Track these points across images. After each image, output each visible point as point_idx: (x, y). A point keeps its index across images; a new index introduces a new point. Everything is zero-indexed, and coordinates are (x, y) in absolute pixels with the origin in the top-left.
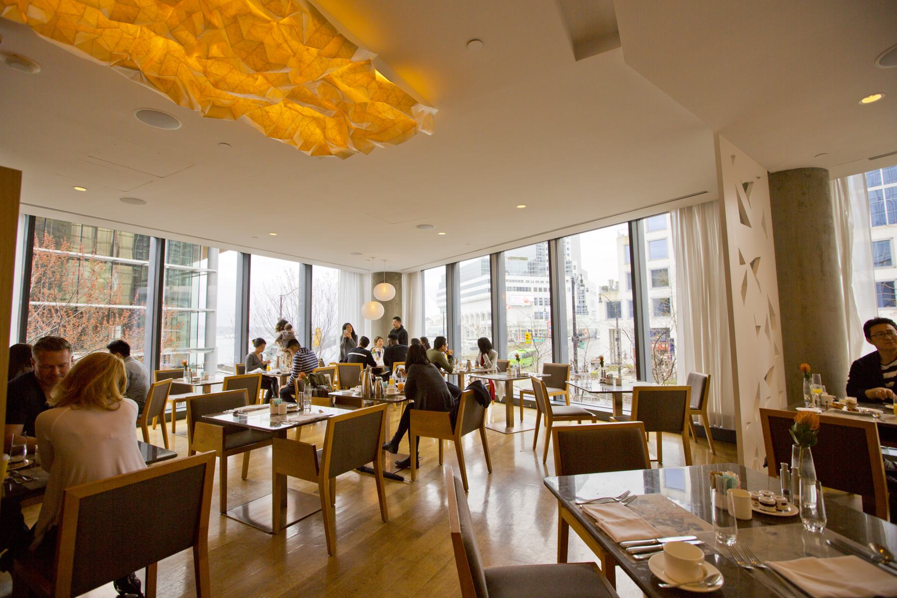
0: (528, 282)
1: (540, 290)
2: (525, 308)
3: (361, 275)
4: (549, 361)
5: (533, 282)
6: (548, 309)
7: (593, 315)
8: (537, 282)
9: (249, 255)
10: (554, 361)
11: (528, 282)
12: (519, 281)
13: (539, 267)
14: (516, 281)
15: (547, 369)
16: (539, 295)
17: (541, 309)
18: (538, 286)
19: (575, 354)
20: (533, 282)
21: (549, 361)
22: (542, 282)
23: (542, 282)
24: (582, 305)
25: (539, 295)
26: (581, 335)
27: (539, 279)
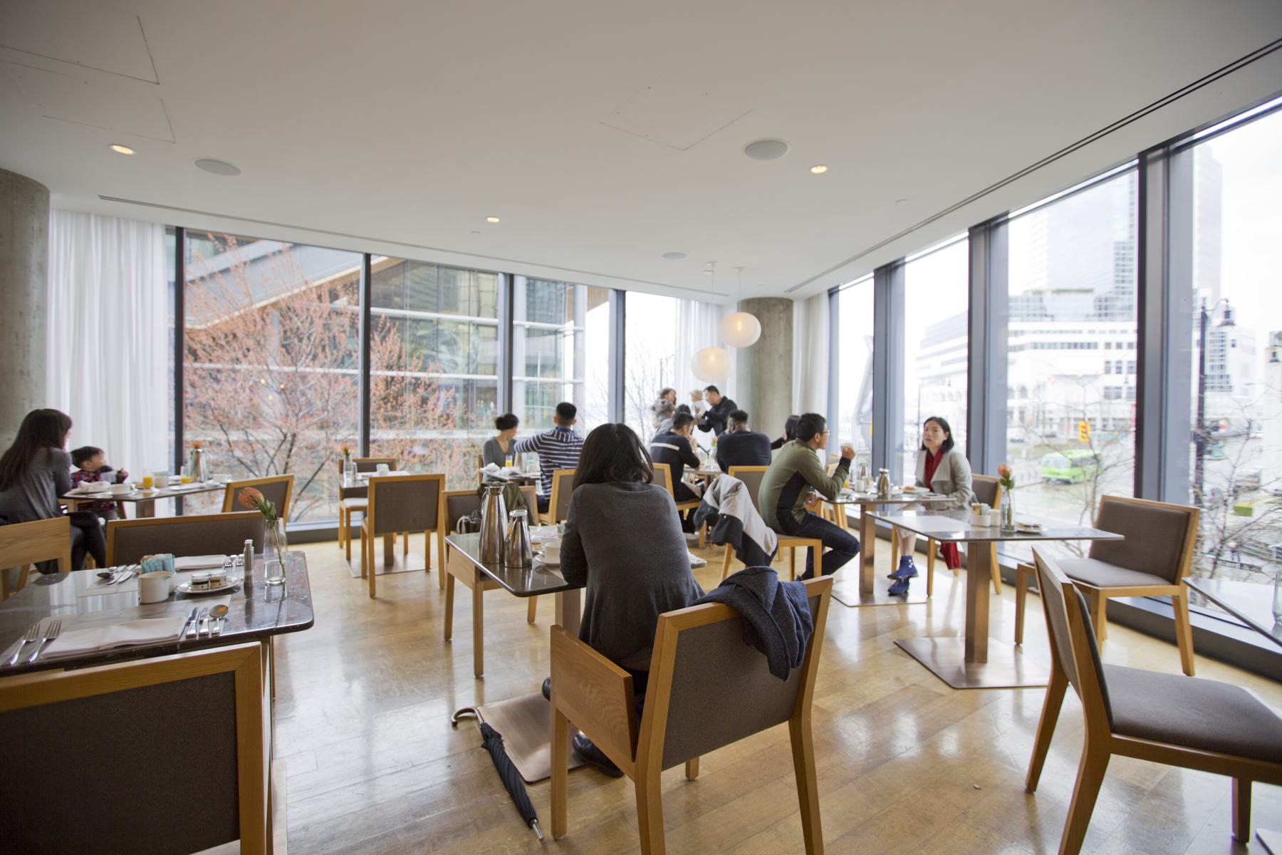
0: (1091, 332)
1: (1119, 346)
2: (1069, 376)
3: (720, 307)
4: (1122, 489)
5: (1102, 332)
6: (1133, 380)
7: (1245, 392)
8: (1113, 332)
9: (624, 292)
10: (1138, 492)
11: (1091, 332)
12: (1074, 332)
13: (1119, 303)
14: (1067, 332)
15: (1111, 514)
16: (1114, 355)
17: (1115, 380)
18: (1114, 339)
19: (1199, 468)
20: (1102, 332)
21: (1122, 489)
22: (1124, 332)
23: (1124, 332)
24: (1217, 372)
25: (1114, 355)
26: (1216, 428)
27: (1118, 325)
